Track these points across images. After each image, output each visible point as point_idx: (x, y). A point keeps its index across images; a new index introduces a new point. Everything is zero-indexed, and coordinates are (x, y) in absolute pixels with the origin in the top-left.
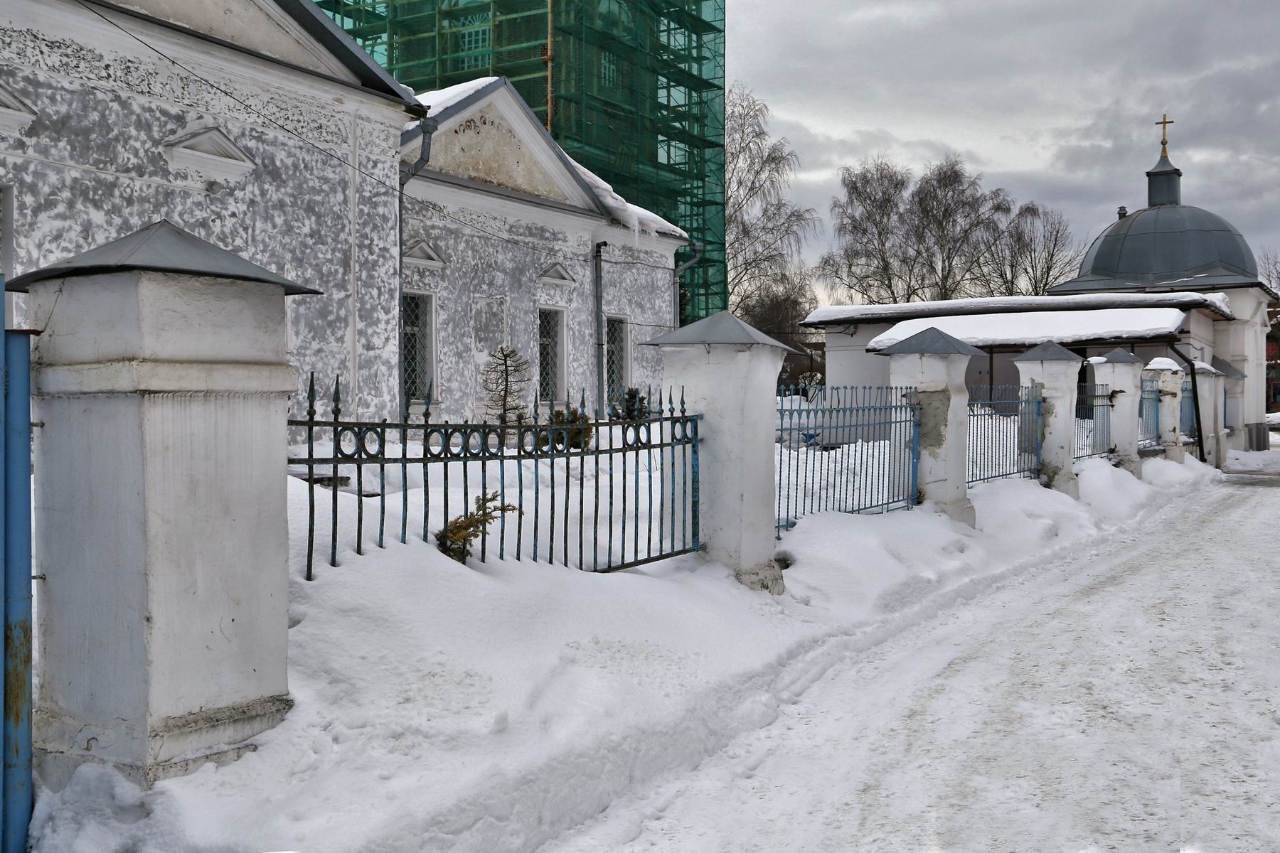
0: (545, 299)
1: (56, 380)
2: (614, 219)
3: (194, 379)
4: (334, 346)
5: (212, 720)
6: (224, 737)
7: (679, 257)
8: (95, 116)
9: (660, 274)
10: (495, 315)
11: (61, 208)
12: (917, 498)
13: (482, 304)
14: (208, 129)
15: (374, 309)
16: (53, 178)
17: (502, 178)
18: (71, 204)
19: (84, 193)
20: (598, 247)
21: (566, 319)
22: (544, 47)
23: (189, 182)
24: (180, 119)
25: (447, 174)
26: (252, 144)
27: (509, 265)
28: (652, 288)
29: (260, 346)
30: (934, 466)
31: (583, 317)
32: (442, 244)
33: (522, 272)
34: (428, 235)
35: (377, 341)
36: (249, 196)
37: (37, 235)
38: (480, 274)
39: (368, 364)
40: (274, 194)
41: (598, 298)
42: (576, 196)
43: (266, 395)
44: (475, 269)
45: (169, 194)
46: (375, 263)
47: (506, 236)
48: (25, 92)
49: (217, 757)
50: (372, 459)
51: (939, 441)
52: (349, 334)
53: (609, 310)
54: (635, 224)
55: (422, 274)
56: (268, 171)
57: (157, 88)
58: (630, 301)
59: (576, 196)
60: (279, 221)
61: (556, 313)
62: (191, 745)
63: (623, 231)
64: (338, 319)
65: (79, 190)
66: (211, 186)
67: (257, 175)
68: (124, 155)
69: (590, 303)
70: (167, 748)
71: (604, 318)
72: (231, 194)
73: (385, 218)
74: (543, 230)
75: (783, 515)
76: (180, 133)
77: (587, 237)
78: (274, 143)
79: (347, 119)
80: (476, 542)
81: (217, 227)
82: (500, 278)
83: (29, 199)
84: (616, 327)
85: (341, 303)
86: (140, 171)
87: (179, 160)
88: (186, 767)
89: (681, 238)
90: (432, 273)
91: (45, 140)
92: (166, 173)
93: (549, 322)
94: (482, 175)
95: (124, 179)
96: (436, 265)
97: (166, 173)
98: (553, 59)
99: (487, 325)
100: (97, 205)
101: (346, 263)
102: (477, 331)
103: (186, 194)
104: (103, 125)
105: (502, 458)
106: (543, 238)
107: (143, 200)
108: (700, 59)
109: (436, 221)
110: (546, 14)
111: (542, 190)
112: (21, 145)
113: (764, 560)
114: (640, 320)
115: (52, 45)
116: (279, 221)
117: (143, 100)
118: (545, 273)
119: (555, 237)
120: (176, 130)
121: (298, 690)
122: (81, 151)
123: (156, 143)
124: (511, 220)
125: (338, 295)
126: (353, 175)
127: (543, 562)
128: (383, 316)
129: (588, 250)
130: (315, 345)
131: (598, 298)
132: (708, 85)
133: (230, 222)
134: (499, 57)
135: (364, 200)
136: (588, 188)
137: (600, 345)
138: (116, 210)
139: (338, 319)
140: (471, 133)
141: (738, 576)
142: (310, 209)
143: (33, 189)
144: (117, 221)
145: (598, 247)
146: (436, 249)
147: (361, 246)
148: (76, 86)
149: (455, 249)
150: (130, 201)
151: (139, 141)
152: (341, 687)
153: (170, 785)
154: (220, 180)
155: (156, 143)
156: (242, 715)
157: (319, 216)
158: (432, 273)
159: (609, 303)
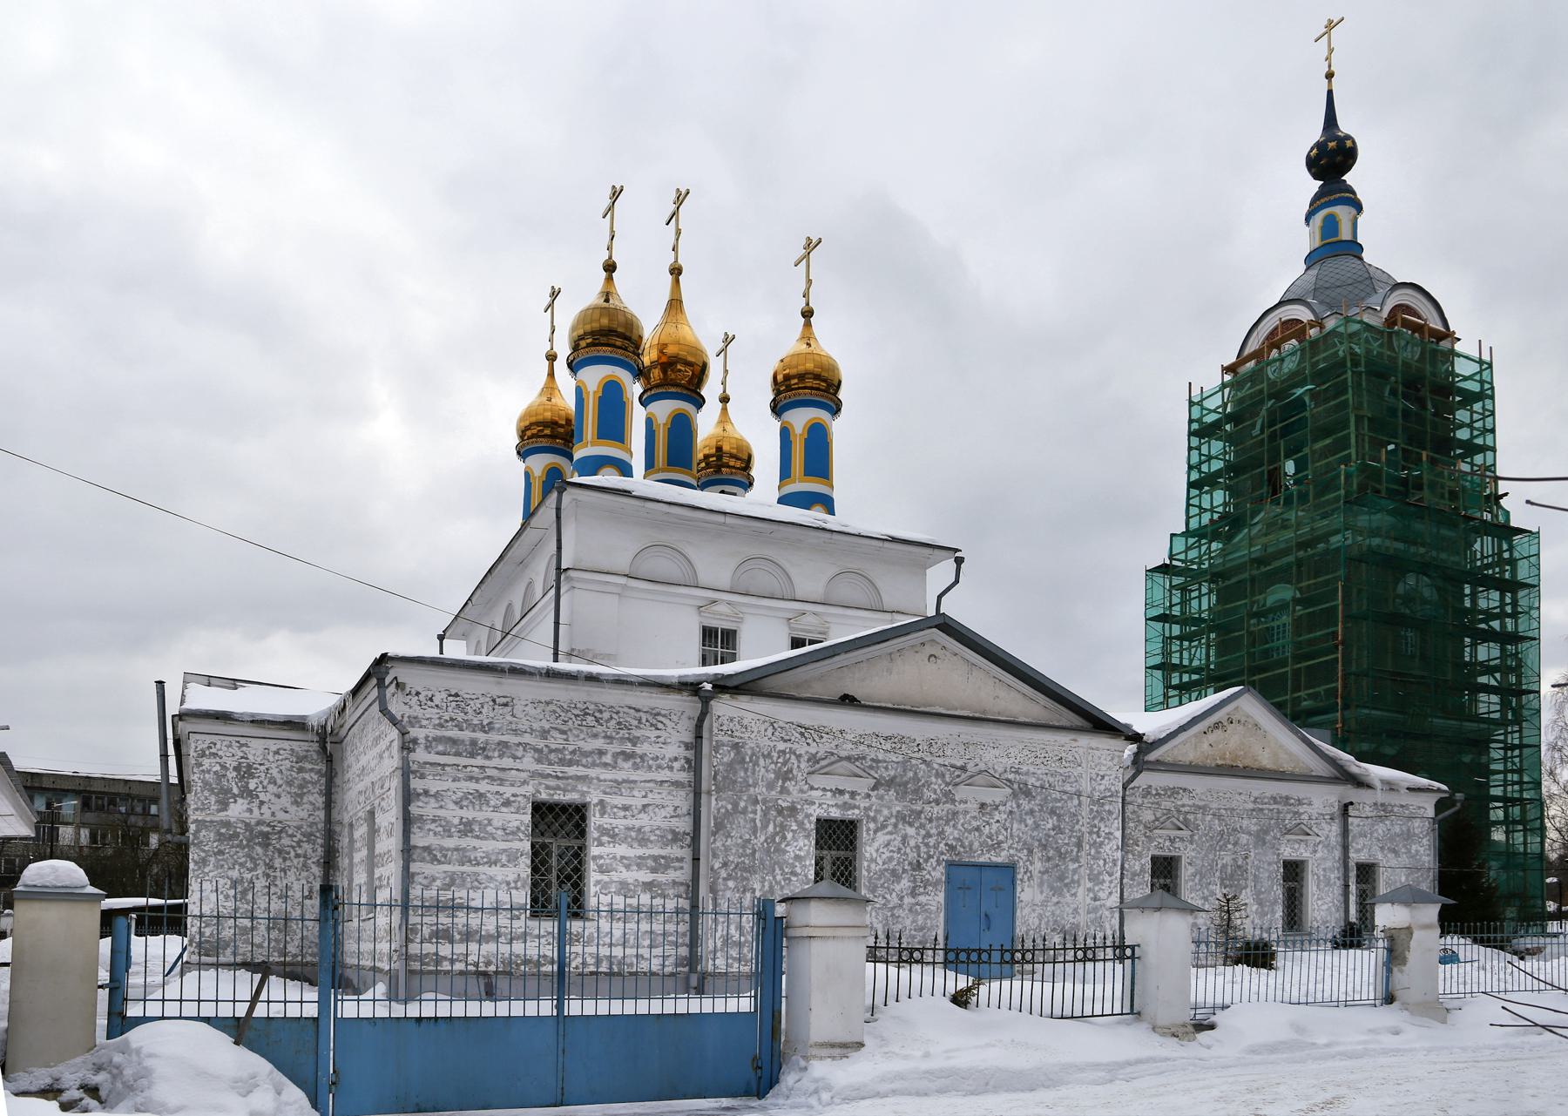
0: (1288, 853)
1: (791, 932)
2: (1359, 783)
3: (829, 932)
4: (1069, 898)
5: (833, 1046)
6: (837, 1051)
7: (1440, 806)
8: (911, 774)
9: (1417, 823)
10: (1239, 867)
11: (890, 828)
12: (1389, 999)
13: (1228, 859)
14: (980, 772)
15: (1100, 873)
16: (886, 812)
17: (1247, 762)
18: (895, 826)
19: (903, 819)
20: (1345, 808)
21: (1311, 867)
22: (1335, 634)
23: (969, 805)
24: (963, 768)
25: (1196, 766)
26: (1011, 776)
27: (1254, 828)
28: (1408, 836)
29: (857, 921)
30: (1401, 978)
31: (1329, 864)
32: (1191, 817)
33: (1266, 832)
34: (1179, 811)
35: (1102, 895)
36: (1008, 808)
37: (876, 845)
38: (1225, 838)
39: (1095, 910)
40: (1025, 804)
41: (1345, 848)
42: (1320, 768)
43: (858, 938)
44: (1221, 833)
45: (955, 814)
46: (1102, 843)
47: (1251, 806)
48: (871, 767)
49: (833, 1058)
50: (917, 962)
51: (1404, 961)
52: (1081, 891)
53: (1357, 856)
54: (1378, 785)
55: (1172, 841)
56: (1025, 791)
57: (948, 753)
58: (1382, 848)
59: (1320, 768)
60: (1030, 822)
61: (1303, 862)
62: (825, 1052)
63: (1370, 791)
64: (1073, 881)
65: (901, 817)
66: (983, 806)
67: (1015, 795)
68: (928, 794)
69: (1338, 853)
70: (814, 1051)
71: (1352, 864)
72: (997, 808)
73: (1110, 812)
74: (1287, 798)
75: (1193, 999)
76: (964, 776)
77: (1333, 799)
78: (1027, 773)
79: (1081, 751)
80: (974, 999)
81: (986, 830)
82: (1244, 838)
83: (872, 826)
84: (1366, 872)
85: (1075, 871)
86: (937, 802)
87: (961, 793)
88: (821, 1058)
89: (1439, 790)
90: (1182, 839)
91: (881, 792)
92: (953, 801)
93: (1293, 872)
94: (1229, 762)
95: (927, 808)
96: (1185, 833)
97: (953, 801)
98: (1343, 643)
99: (1232, 876)
100: (911, 825)
101: (1079, 845)
102: (1222, 880)
103: (966, 812)
104: (916, 778)
105: (887, 962)
106: (1287, 804)
107: (939, 819)
108: (1515, 615)
109: (1186, 801)
110: (1336, 607)
111: (1287, 767)
112: (869, 796)
113: (1180, 1021)
114: (1394, 863)
115: (886, 739)
116: (1030, 822)
117: (940, 761)
118: (1289, 832)
119: (1300, 802)
120: (962, 774)
121: (867, 1041)
122: (901, 796)
123: (947, 784)
124: (1256, 794)
125: (1072, 866)
126: (1085, 786)
127: (1015, 1012)
128: (1107, 878)
129: (1336, 809)
130: (1055, 899)
131: (1345, 848)
132: (1516, 638)
133: (995, 826)
134: (1298, 645)
135: (1093, 802)
136: (1332, 761)
137: (1347, 886)
138: (922, 826)
139: (1073, 881)
140: (1219, 732)
141: (1154, 1029)
142: (1053, 812)
143: (874, 820)
144: (923, 832)
145: (1345, 808)
146: (1186, 823)
147: (1090, 833)
148: (900, 758)
149: (1203, 820)
150: (930, 820)
151: (937, 784)
152: (884, 1041)
153: (814, 1062)
154: (989, 801)
155: (947, 784)
156: (844, 1046)
157: (1059, 816)
158: (1182, 839)
159: (1358, 851)
